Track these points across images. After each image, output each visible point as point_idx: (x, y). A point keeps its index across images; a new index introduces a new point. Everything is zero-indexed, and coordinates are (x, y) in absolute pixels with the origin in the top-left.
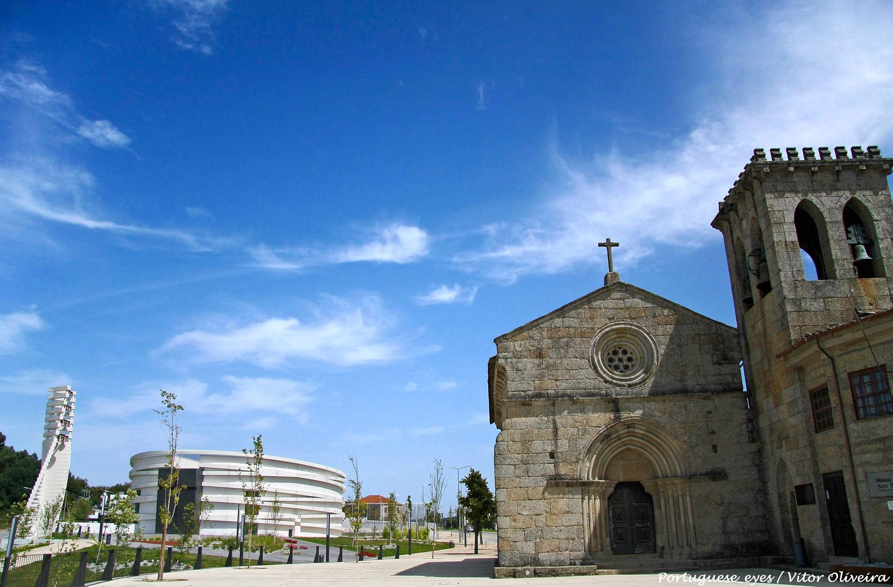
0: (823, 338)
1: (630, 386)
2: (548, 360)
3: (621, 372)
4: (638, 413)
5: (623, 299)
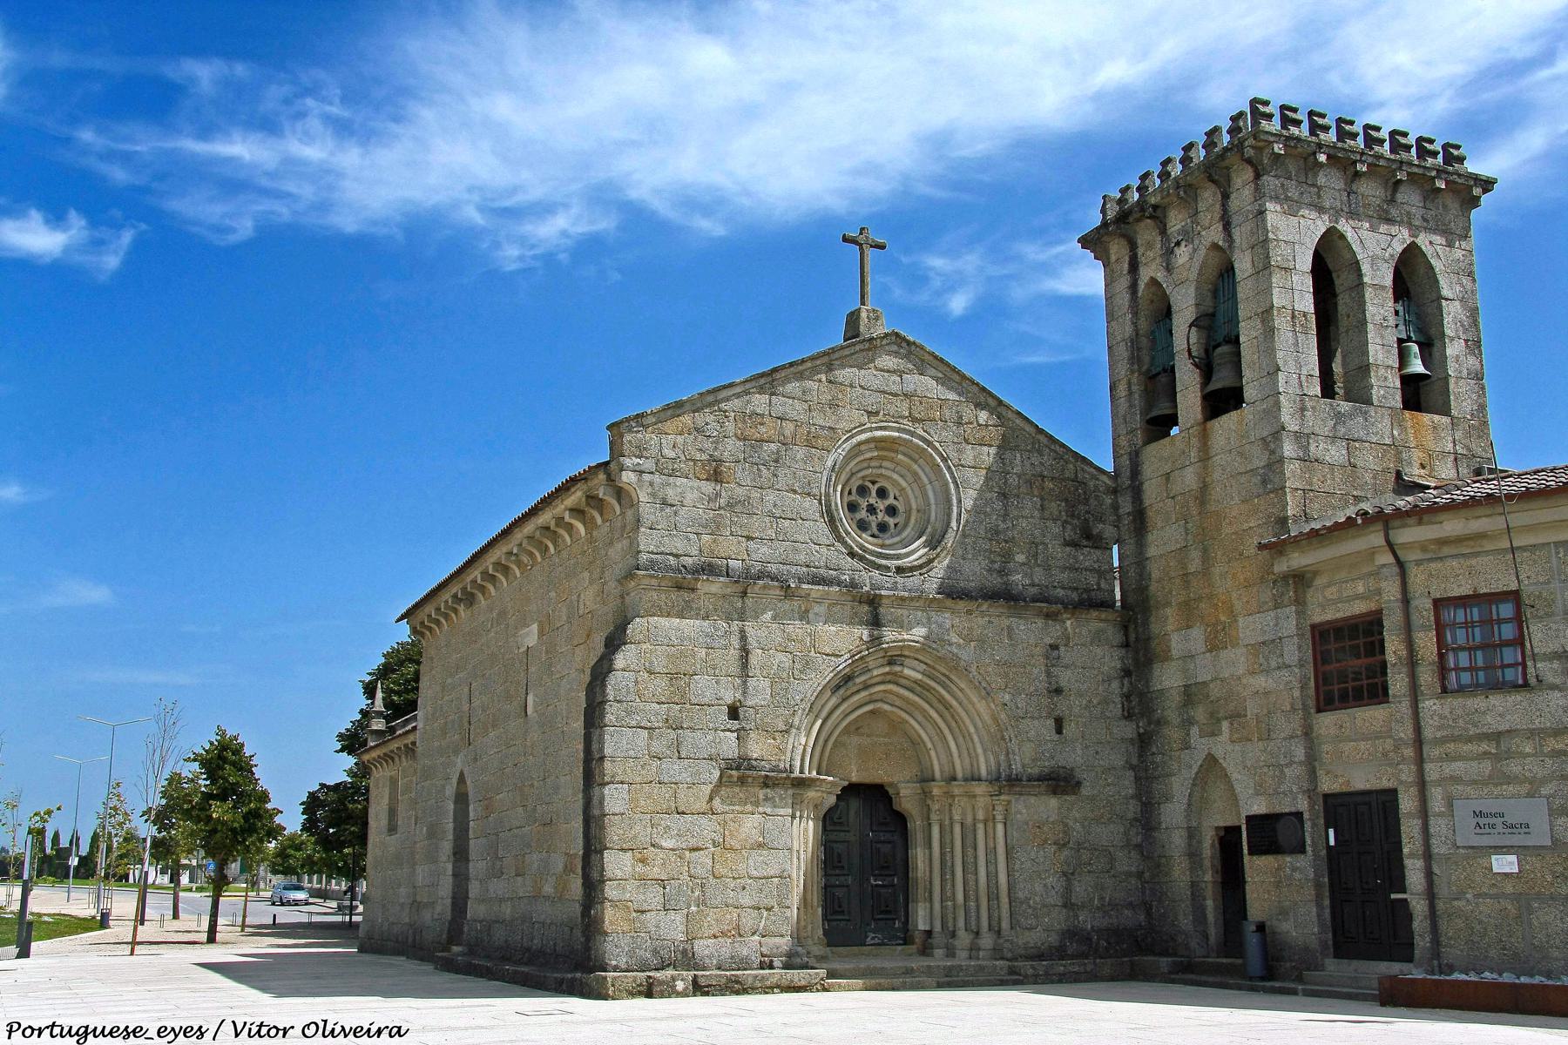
0: (1397, 523)
1: (900, 570)
2: (730, 491)
3: (873, 536)
4: (919, 632)
5: (900, 373)
